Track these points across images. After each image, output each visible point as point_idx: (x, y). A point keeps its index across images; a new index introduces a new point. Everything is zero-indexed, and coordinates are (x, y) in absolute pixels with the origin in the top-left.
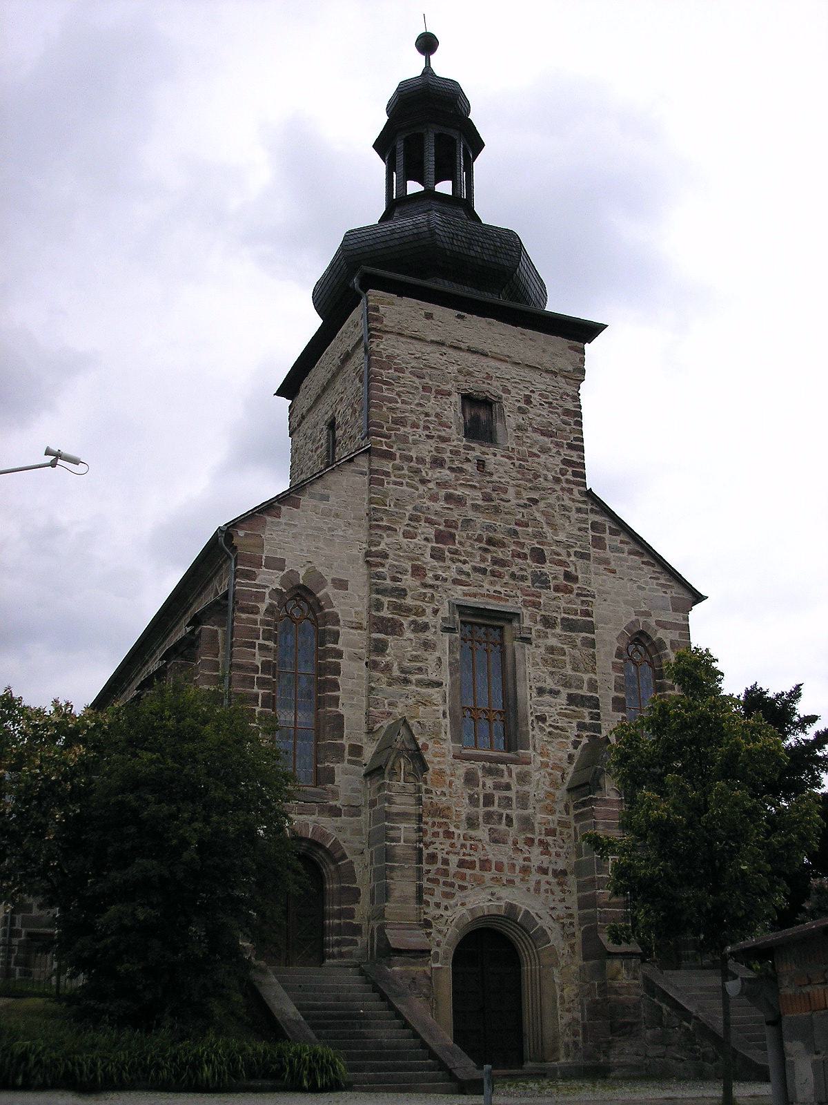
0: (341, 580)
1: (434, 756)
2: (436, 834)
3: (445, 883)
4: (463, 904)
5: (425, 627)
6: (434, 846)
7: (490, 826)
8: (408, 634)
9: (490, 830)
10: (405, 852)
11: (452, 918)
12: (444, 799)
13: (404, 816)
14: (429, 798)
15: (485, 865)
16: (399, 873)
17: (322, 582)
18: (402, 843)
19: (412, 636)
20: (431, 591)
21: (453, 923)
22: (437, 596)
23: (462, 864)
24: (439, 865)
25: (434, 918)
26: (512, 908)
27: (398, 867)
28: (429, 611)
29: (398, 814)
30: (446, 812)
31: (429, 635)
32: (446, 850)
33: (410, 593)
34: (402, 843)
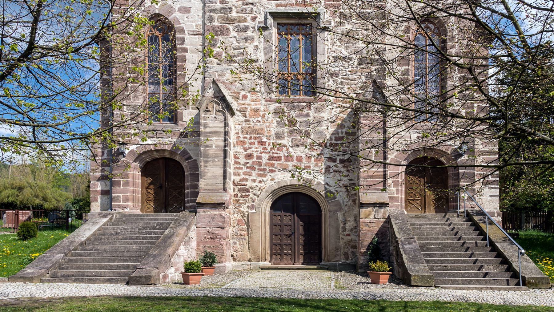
0: (185, 8)
1: (251, 101)
2: (252, 144)
3: (259, 169)
4: (272, 180)
5: (246, 29)
6: (251, 150)
7: (292, 137)
8: (233, 34)
9: (292, 139)
10: (215, 153)
11: (263, 187)
12: (259, 124)
13: (215, 133)
14: (248, 124)
15: (289, 158)
16: (211, 163)
17: (171, 10)
18: (214, 147)
19: (236, 35)
20: (251, 6)
21: (264, 190)
22: (255, 9)
23: (271, 158)
24: (295, 162)
25: (251, 188)
26: (309, 181)
27: (211, 160)
28: (249, 18)
29: (210, 133)
30: (260, 131)
31: (250, 33)
32: (259, 151)
33: (234, 9)
34: (214, 147)
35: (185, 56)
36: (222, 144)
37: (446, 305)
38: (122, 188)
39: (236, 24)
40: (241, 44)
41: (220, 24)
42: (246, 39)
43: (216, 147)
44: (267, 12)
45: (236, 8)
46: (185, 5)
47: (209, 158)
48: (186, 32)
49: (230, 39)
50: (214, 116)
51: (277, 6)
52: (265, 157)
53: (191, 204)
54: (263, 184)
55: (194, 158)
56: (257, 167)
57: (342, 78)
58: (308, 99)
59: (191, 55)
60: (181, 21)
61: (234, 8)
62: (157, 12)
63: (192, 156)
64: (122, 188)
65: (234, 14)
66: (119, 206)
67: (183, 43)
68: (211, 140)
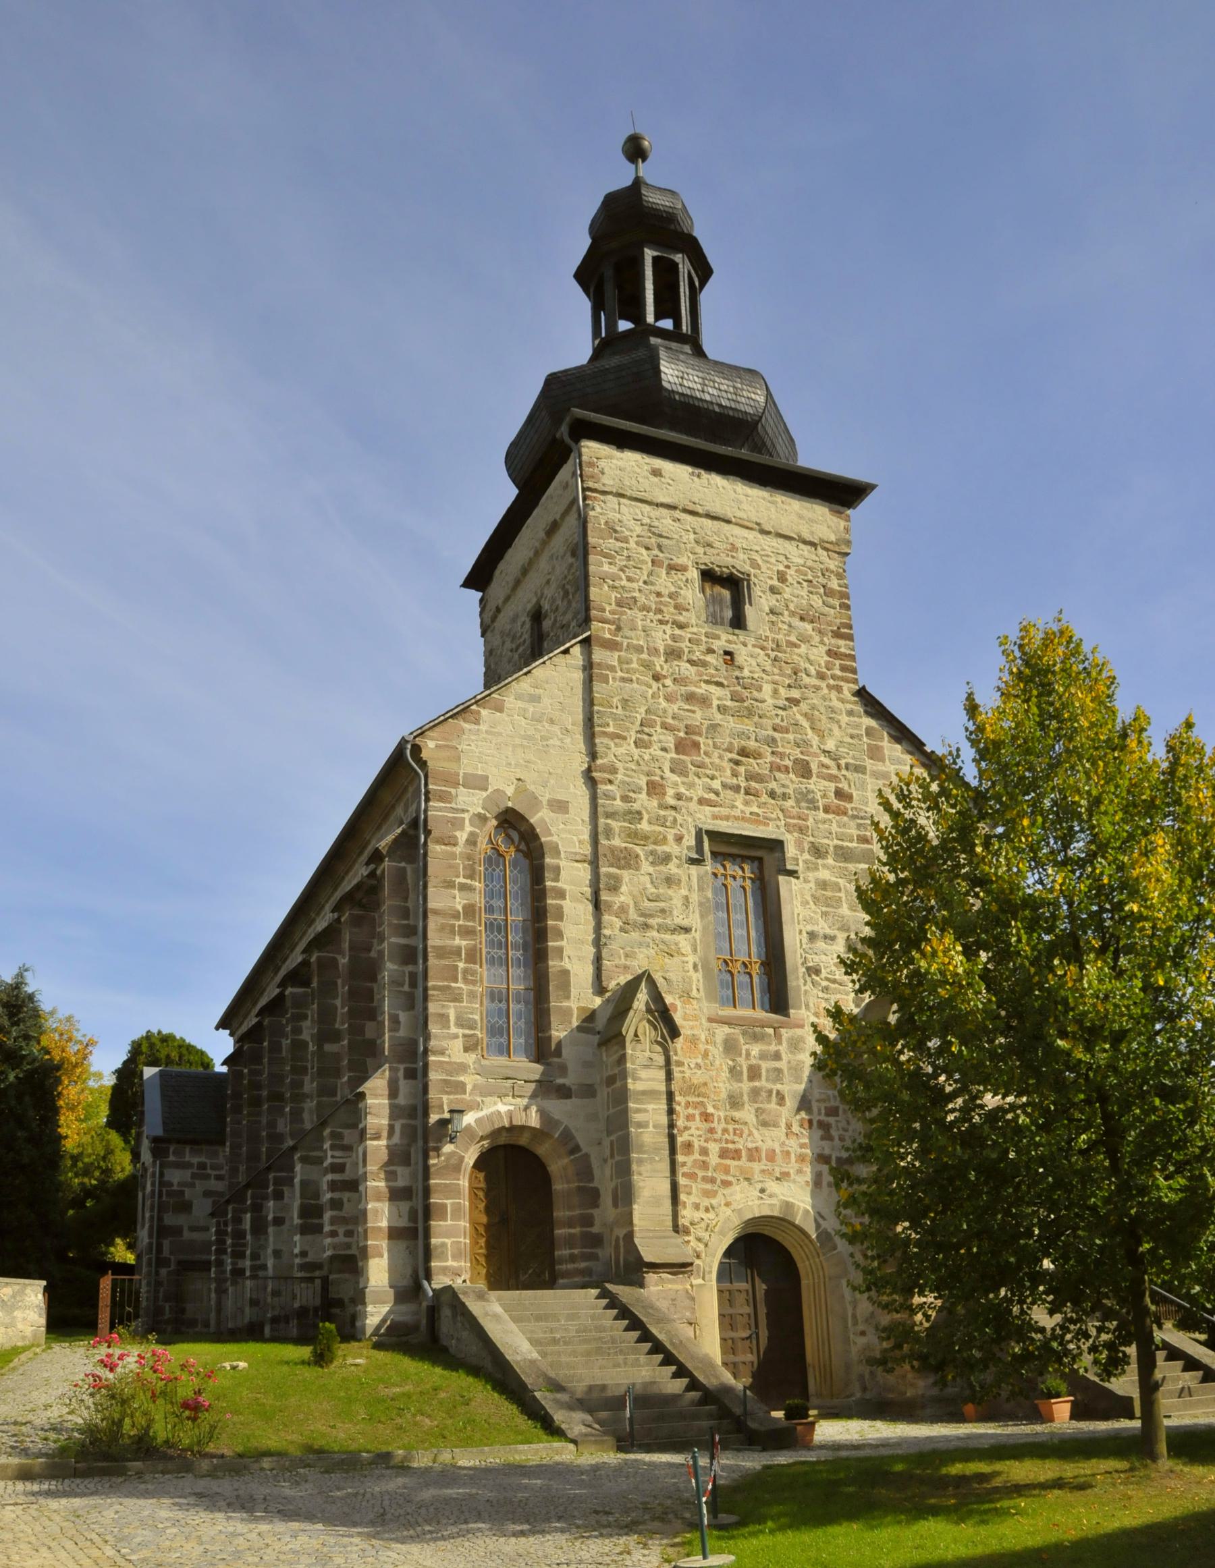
0: (559, 801)
3: (704, 1179)
5: (667, 859)
7: (756, 1105)
8: (646, 867)
9: (757, 1110)
13: (650, 1094)
19: (651, 869)
20: (673, 813)
28: (670, 838)
29: (644, 1093)
30: (702, 1090)
31: (672, 868)
34: (651, 1129)
35: (561, 907)
36: (664, 1120)
37: (956, 1469)
38: (449, 1222)
39: (651, 847)
40: (661, 891)
41: (624, 845)
42: (669, 881)
43: (654, 1127)
44: (701, 829)
45: (648, 813)
46: (559, 797)
47: (644, 1152)
48: (563, 855)
49: (642, 878)
50: (648, 1054)
51: (715, 817)
52: (714, 1148)
53: (583, 1265)
54: (711, 1215)
55: (585, 1149)
56: (700, 1174)
57: (827, 979)
58: (778, 1022)
59: (574, 904)
60: (553, 830)
61: (644, 813)
62: (510, 804)
63: (581, 1144)
64: (449, 1222)
65: (644, 826)
66: (445, 1270)
67: (557, 879)
68: (646, 1111)
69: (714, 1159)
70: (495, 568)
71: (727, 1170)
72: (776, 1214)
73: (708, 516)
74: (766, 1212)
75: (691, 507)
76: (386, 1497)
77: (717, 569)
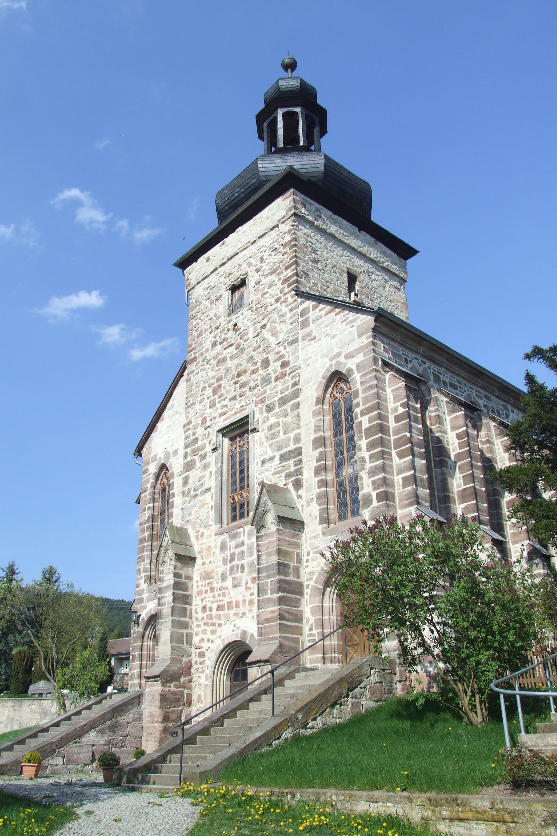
34: (167, 606)
69: (214, 612)
70: (368, 233)
71: (219, 617)
72: (239, 639)
73: (229, 259)
74: (235, 639)
75: (204, 276)
76: (300, 802)
77: (235, 283)
